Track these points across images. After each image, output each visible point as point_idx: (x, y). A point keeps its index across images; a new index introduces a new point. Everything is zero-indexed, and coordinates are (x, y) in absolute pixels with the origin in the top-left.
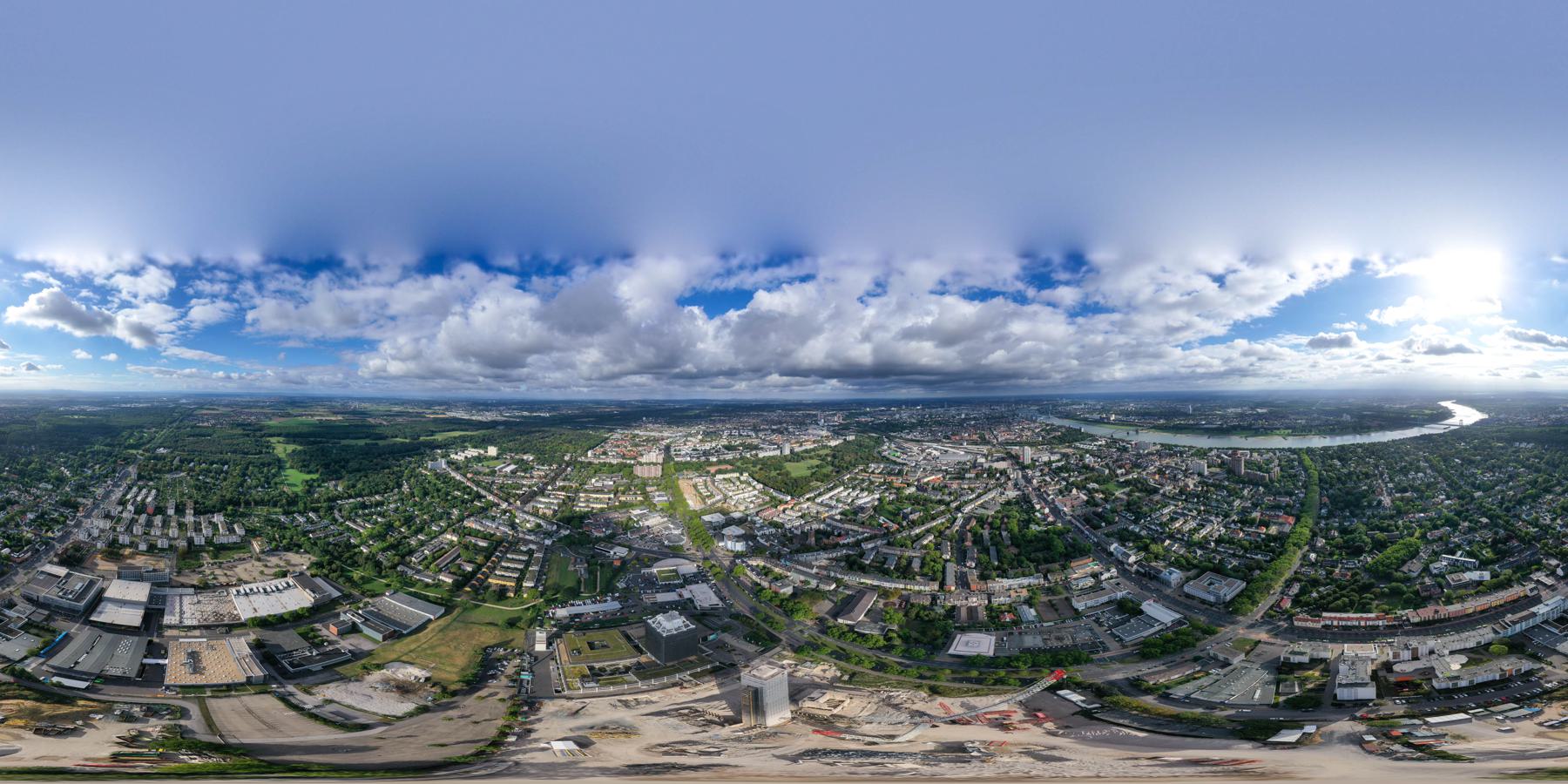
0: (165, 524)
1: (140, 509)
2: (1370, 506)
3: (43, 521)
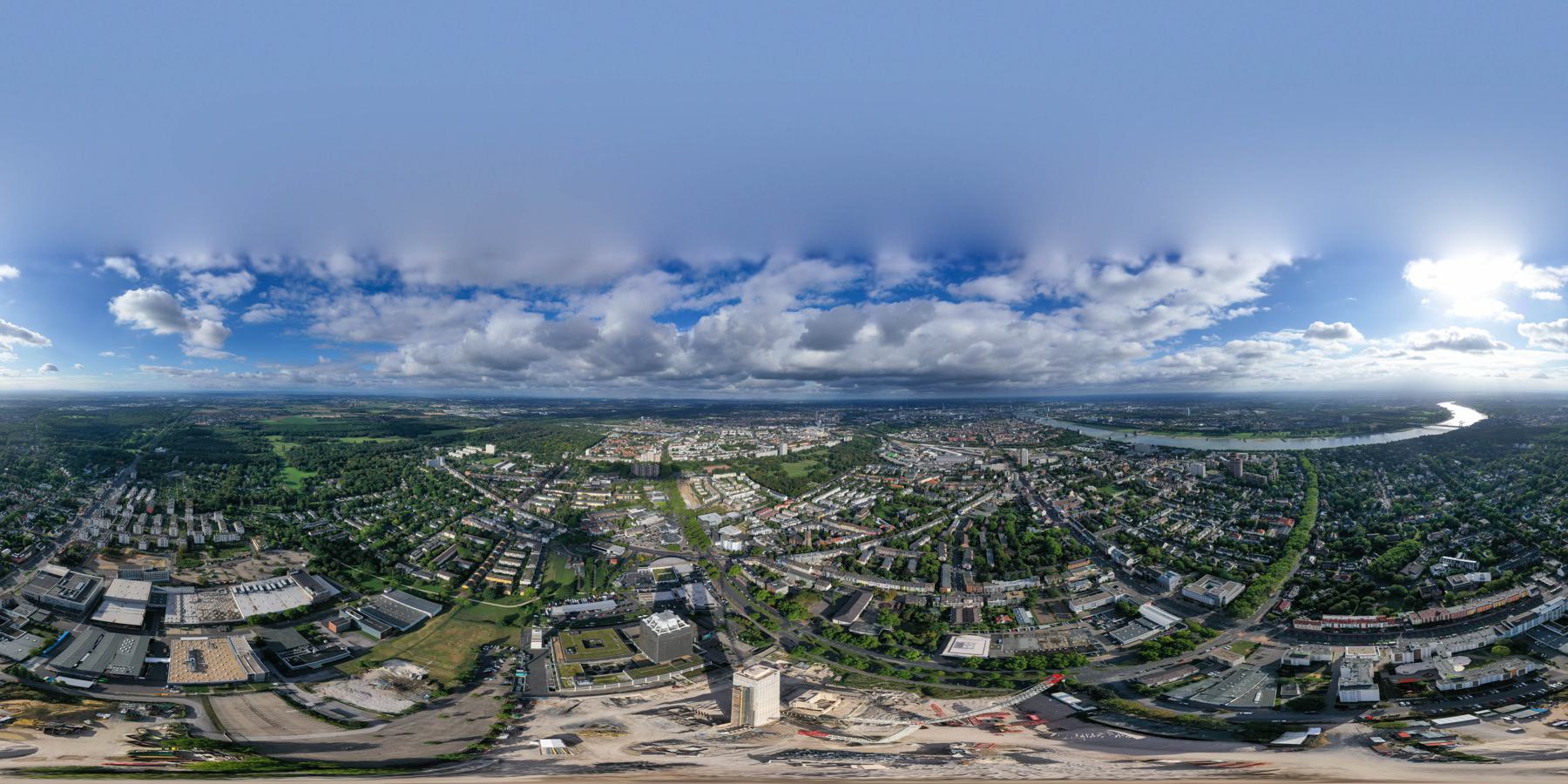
1: (140, 508)
3: (43, 521)
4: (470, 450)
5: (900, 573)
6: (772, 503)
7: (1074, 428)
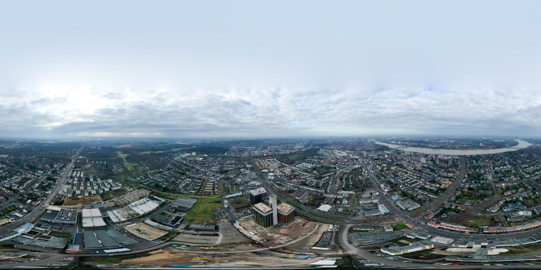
0: (91, 184)
1: (80, 179)
2: (483, 179)
3: (43, 188)
4: (187, 155)
5: (318, 187)
6: (283, 166)
7: (386, 145)
